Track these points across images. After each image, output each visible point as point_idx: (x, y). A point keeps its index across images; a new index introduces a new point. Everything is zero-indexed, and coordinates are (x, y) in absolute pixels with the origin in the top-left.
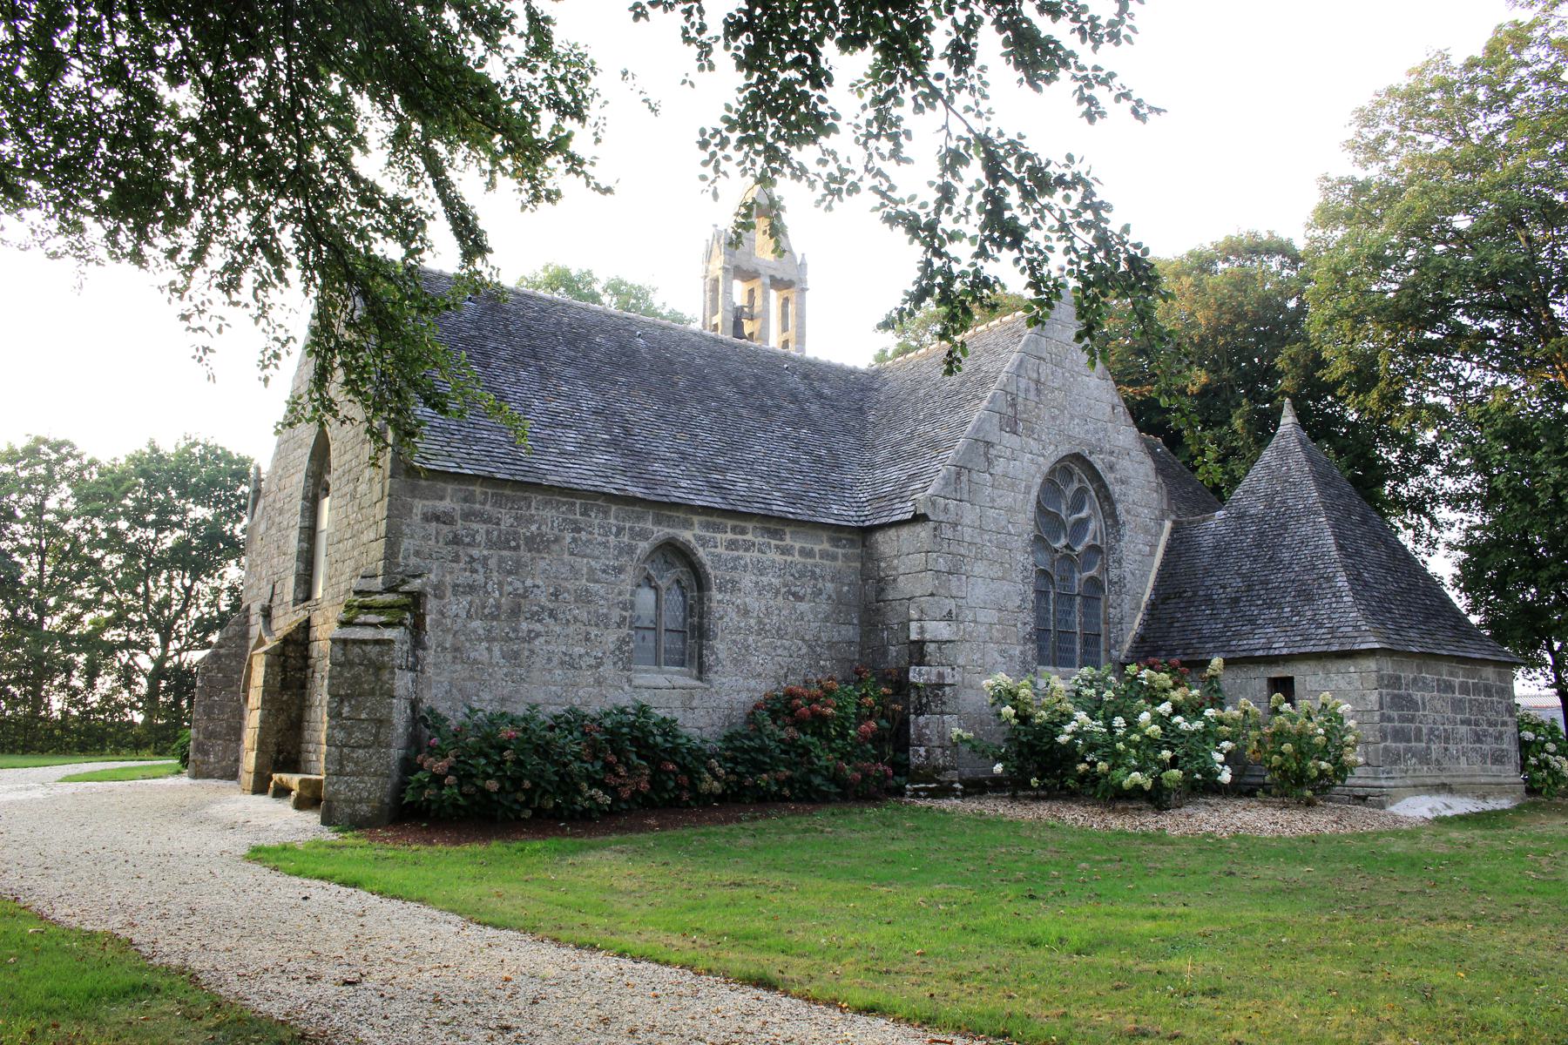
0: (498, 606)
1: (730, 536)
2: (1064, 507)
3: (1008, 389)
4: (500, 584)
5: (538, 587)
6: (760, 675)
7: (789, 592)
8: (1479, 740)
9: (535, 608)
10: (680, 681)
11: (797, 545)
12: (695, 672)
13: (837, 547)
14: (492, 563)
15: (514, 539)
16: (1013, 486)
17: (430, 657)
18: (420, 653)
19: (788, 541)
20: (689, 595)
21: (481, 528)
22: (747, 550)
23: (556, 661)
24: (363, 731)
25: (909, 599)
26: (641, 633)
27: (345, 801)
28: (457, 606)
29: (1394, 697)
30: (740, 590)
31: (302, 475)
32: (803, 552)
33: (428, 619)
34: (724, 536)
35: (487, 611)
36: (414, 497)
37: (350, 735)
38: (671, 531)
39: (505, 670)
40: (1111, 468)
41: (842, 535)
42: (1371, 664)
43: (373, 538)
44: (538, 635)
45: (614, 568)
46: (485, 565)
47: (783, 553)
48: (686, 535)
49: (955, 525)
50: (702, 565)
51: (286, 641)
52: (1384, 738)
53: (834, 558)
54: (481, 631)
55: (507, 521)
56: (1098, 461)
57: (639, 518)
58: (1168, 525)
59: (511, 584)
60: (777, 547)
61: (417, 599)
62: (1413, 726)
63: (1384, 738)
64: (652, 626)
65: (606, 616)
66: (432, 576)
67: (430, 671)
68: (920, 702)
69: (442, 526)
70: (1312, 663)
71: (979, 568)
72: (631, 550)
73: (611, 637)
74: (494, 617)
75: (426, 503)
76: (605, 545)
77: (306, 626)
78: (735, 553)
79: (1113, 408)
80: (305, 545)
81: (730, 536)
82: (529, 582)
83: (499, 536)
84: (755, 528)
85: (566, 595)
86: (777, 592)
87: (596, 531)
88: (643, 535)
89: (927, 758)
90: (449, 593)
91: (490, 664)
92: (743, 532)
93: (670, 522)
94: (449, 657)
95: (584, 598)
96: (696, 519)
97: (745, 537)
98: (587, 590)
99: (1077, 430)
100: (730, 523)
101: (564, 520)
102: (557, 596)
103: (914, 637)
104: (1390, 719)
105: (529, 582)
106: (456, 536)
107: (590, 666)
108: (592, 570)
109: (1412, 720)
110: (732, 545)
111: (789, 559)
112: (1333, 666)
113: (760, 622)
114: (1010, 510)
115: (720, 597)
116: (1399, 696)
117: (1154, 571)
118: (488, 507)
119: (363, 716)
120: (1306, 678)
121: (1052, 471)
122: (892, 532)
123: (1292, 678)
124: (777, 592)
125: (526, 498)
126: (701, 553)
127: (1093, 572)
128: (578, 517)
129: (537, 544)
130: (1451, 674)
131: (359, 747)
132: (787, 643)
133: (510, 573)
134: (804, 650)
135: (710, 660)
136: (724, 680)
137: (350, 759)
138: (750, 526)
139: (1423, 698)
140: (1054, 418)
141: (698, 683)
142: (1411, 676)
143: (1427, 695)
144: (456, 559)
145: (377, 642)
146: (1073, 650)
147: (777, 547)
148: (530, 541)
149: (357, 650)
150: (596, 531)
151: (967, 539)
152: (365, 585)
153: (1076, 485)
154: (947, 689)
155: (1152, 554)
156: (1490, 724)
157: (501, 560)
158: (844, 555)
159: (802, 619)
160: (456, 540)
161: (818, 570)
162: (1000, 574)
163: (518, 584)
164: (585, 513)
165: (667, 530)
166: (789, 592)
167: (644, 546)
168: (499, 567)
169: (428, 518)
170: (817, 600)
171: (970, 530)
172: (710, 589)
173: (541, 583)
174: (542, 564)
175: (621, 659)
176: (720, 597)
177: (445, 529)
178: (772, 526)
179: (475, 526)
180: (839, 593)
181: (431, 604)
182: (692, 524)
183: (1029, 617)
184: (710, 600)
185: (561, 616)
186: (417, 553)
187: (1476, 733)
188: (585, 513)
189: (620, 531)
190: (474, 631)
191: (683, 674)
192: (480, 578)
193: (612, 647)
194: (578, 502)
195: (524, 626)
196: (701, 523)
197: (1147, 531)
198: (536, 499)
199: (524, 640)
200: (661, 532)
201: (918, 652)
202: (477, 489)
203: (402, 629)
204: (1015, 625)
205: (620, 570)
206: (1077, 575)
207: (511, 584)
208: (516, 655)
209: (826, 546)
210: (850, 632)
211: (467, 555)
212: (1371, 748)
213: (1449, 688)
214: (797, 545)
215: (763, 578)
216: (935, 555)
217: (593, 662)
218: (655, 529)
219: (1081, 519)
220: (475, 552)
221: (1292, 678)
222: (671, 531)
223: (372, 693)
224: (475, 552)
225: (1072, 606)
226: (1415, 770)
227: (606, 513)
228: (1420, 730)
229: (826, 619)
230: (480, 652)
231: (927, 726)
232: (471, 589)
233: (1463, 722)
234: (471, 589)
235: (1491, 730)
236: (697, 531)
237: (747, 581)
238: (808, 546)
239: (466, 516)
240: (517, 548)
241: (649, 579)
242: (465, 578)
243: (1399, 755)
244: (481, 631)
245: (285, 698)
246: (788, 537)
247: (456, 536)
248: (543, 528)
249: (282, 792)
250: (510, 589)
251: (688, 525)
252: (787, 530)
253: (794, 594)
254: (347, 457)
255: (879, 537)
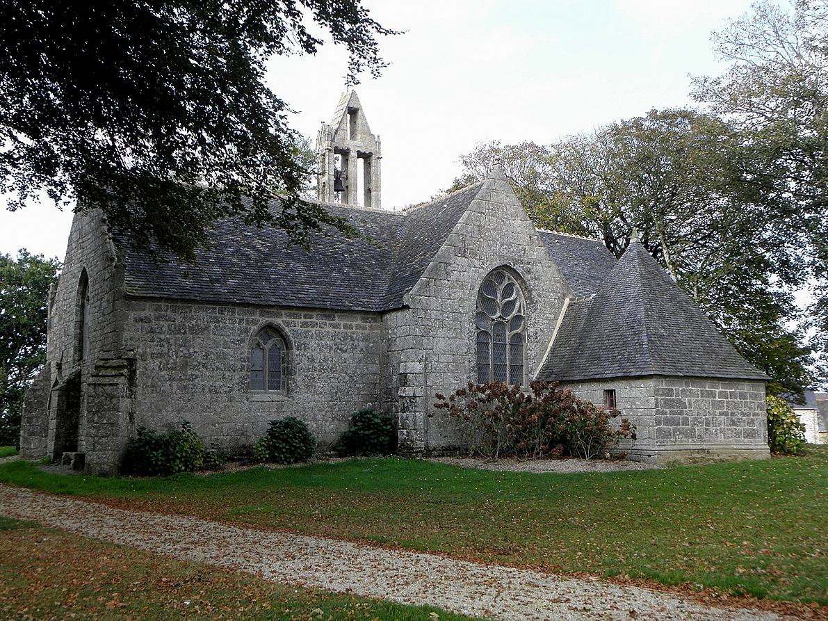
0: (175, 363)
1: (303, 320)
2: (499, 295)
3: (460, 232)
4: (176, 352)
5: (197, 352)
6: (321, 393)
7: (338, 348)
8: (734, 423)
9: (195, 363)
10: (275, 397)
11: (342, 323)
12: (285, 393)
13: (366, 322)
14: (172, 341)
15: (183, 329)
16: (462, 287)
17: (139, 390)
18: (134, 389)
19: (337, 321)
20: (282, 352)
21: (166, 324)
22: (313, 327)
23: (207, 390)
24: (105, 429)
25: (402, 350)
26: (255, 373)
27: (96, 463)
28: (154, 364)
29: (666, 401)
30: (309, 348)
31: (74, 293)
32: (345, 326)
33: (138, 372)
34: (300, 320)
35: (169, 366)
36: (129, 310)
37: (98, 431)
38: (270, 319)
39: (179, 395)
40: (529, 272)
41: (368, 316)
42: (651, 383)
43: (109, 330)
44: (197, 377)
45: (238, 340)
46: (168, 342)
47: (334, 328)
48: (278, 321)
49: (425, 310)
50: (288, 337)
51: (69, 382)
52: (659, 423)
53: (364, 328)
54: (166, 376)
55: (179, 319)
56: (518, 267)
57: (251, 314)
58: (567, 301)
59: (182, 351)
60: (330, 324)
61: (131, 362)
62: (681, 417)
63: (659, 423)
64: (261, 369)
65: (233, 365)
66: (139, 350)
67: (139, 398)
68: (404, 406)
69: (144, 324)
70: (624, 382)
71: (441, 333)
72: (247, 331)
73: (237, 377)
74: (173, 369)
75: (135, 313)
76: (233, 328)
77: (79, 375)
78: (306, 329)
79: (530, 237)
80: (78, 331)
81: (303, 320)
82: (191, 350)
83: (175, 328)
84: (317, 315)
85: (212, 355)
86: (331, 348)
87: (228, 322)
88: (254, 322)
89: (407, 436)
90: (149, 357)
91: (172, 393)
92: (311, 317)
93: (269, 314)
94: (150, 390)
95: (222, 357)
96: (283, 312)
97: (311, 320)
98: (223, 353)
99: (504, 251)
100: (303, 313)
101: (210, 317)
102: (207, 357)
103: (402, 371)
104: (663, 413)
105: (191, 350)
106: (152, 329)
107: (226, 392)
108: (225, 342)
109: (681, 413)
110: (304, 325)
111: (337, 330)
112: (634, 383)
113: (321, 364)
114: (461, 299)
115: (298, 353)
116: (671, 400)
117: (557, 329)
118: (168, 313)
119: (105, 422)
120: (623, 390)
121: (490, 274)
122: (394, 314)
123: (615, 390)
124: (331, 348)
125: (189, 307)
126: (287, 330)
127: (518, 331)
128: (218, 315)
129: (196, 330)
130: (713, 387)
131: (103, 437)
132: (337, 376)
133: (181, 346)
134: (347, 378)
135: (292, 386)
136: (300, 396)
137: (99, 443)
138: (314, 314)
139: (689, 401)
140: (490, 246)
141: (287, 398)
142: (681, 389)
143: (693, 400)
144: (152, 341)
145: (111, 385)
146: (505, 375)
147: (330, 324)
148: (192, 329)
149: (100, 389)
150: (228, 322)
151: (433, 317)
152: (105, 355)
153: (506, 282)
154: (418, 398)
155: (556, 319)
156: (744, 415)
157: (177, 339)
158: (371, 327)
159: (346, 362)
160: (152, 331)
161: (354, 336)
162: (454, 335)
163: (186, 351)
164: (221, 312)
165: (267, 319)
166: (338, 348)
167: (254, 328)
168: (175, 343)
169: (136, 321)
170: (354, 352)
171: (435, 312)
172: (292, 349)
173: (198, 350)
174: (198, 340)
175: (242, 387)
176: (298, 353)
177: (146, 325)
178: (327, 313)
179: (162, 323)
180: (367, 347)
181: (139, 364)
182: (282, 315)
183: (474, 358)
184: (292, 354)
185: (209, 367)
186: (132, 339)
187: (732, 420)
188: (221, 312)
189: (241, 321)
190: (163, 376)
191: (278, 394)
192: (165, 349)
193: (237, 381)
194: (217, 307)
195: (189, 372)
196: (286, 314)
197: (552, 306)
198: (194, 307)
199: (189, 380)
200: (264, 320)
201: (404, 380)
202: (163, 304)
203: (123, 378)
204: (464, 363)
205: (242, 341)
206: (507, 333)
207: (182, 351)
208: (185, 388)
209: (359, 322)
210: (374, 368)
211: (158, 338)
212: (651, 429)
213: (712, 395)
214: (342, 323)
215: (322, 342)
216: (413, 327)
217: (227, 389)
218: (261, 319)
219: (510, 301)
220: (162, 336)
221: (615, 390)
222: (270, 319)
223: (109, 409)
224: (162, 336)
225: (505, 350)
226: (682, 441)
227: (233, 312)
228: (687, 419)
229: (360, 362)
230: (166, 387)
231: (407, 418)
232: (161, 355)
233: (721, 414)
234: (161, 355)
235: (744, 418)
236: (284, 319)
237: (313, 343)
238: (349, 323)
239: (157, 319)
240: (184, 333)
241: (258, 345)
242: (157, 350)
243: (670, 433)
244: (166, 376)
245: (69, 413)
246: (337, 318)
247: (152, 329)
248: (199, 322)
249: (67, 461)
250: (182, 354)
251: (279, 315)
252: (336, 315)
253: (340, 349)
254: (96, 286)
255: (388, 316)
